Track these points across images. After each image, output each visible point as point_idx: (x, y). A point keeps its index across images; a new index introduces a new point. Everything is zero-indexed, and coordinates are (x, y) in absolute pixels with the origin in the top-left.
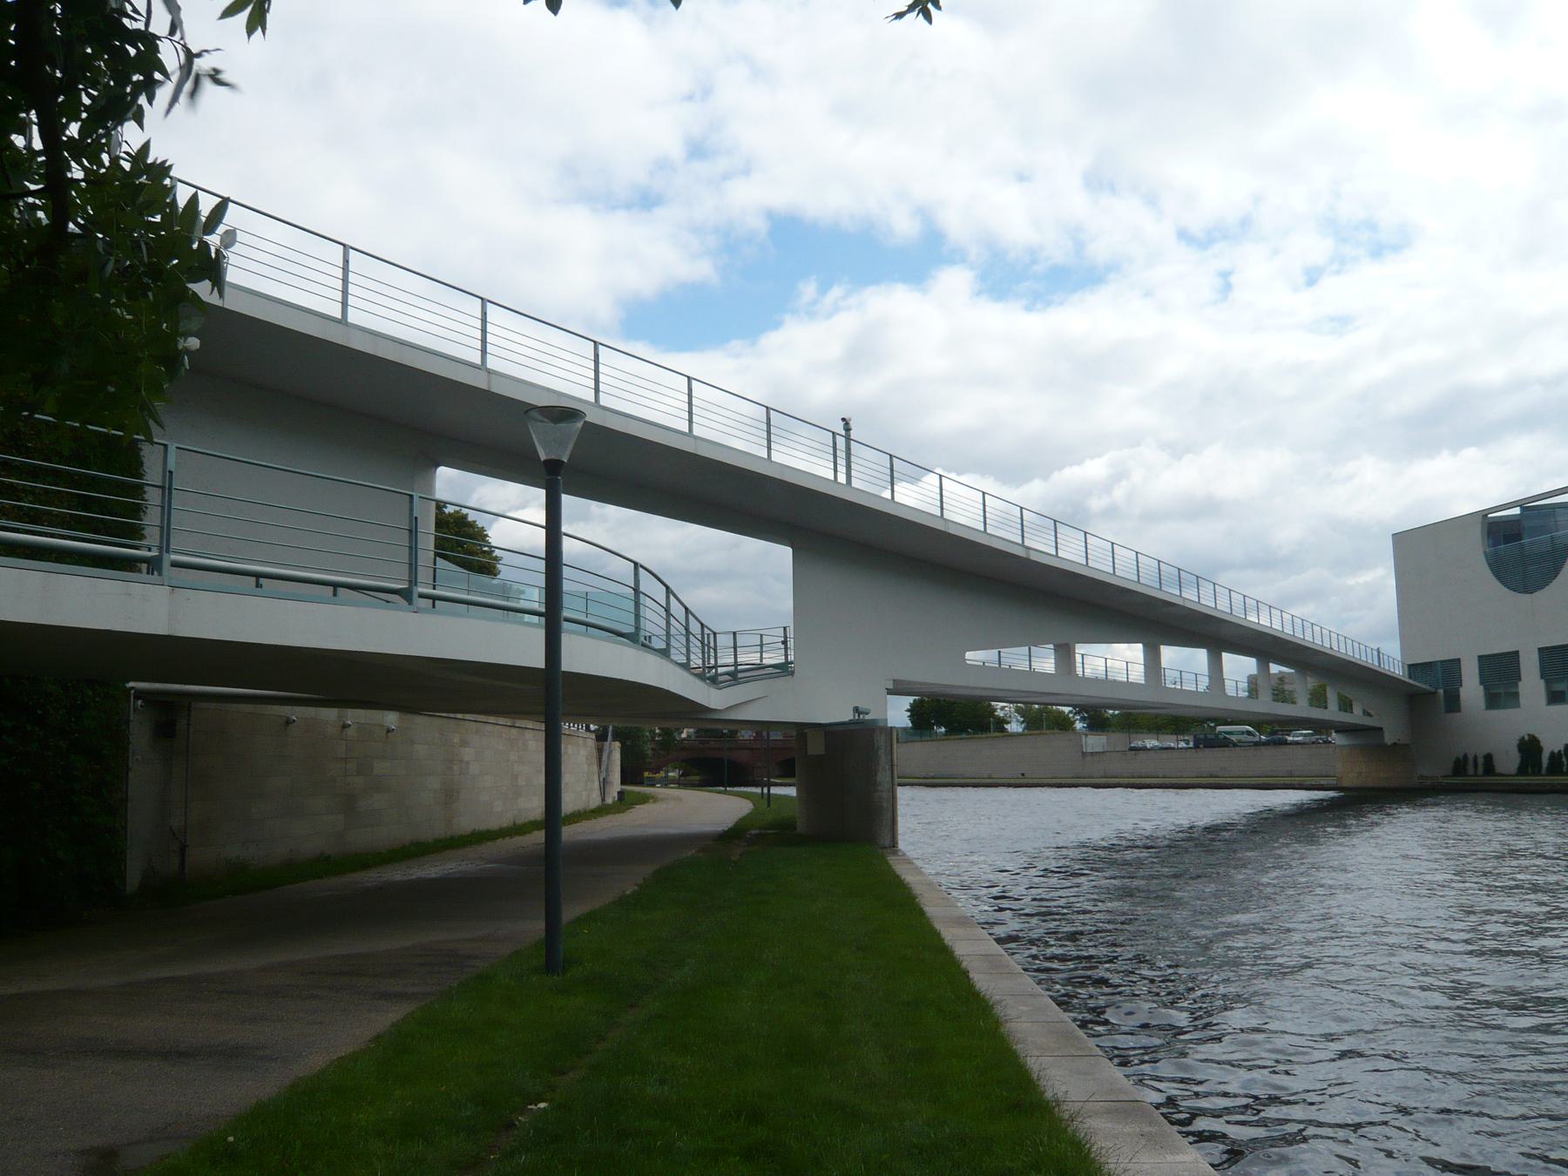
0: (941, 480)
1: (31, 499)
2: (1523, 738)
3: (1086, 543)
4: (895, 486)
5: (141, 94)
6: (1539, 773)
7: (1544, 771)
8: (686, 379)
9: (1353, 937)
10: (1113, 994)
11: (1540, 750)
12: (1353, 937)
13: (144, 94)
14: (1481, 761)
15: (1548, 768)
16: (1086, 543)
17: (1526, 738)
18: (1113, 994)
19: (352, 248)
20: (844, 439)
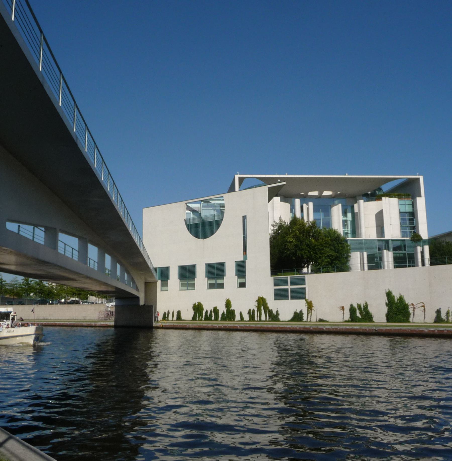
0: (65, 246)
1: (352, 410)
2: (196, 303)
3: (34, 234)
4: (386, 339)
5: (232, 310)
6: (218, 321)
7: (219, 319)
8: (64, 244)
9: (354, 368)
10: (350, 370)
11: (202, 309)
12: (354, 368)
13: (231, 309)
14: (175, 314)
15: (221, 318)
16: (34, 234)
17: (197, 304)
18: (350, 370)
19: (68, 245)
20: (77, 252)
